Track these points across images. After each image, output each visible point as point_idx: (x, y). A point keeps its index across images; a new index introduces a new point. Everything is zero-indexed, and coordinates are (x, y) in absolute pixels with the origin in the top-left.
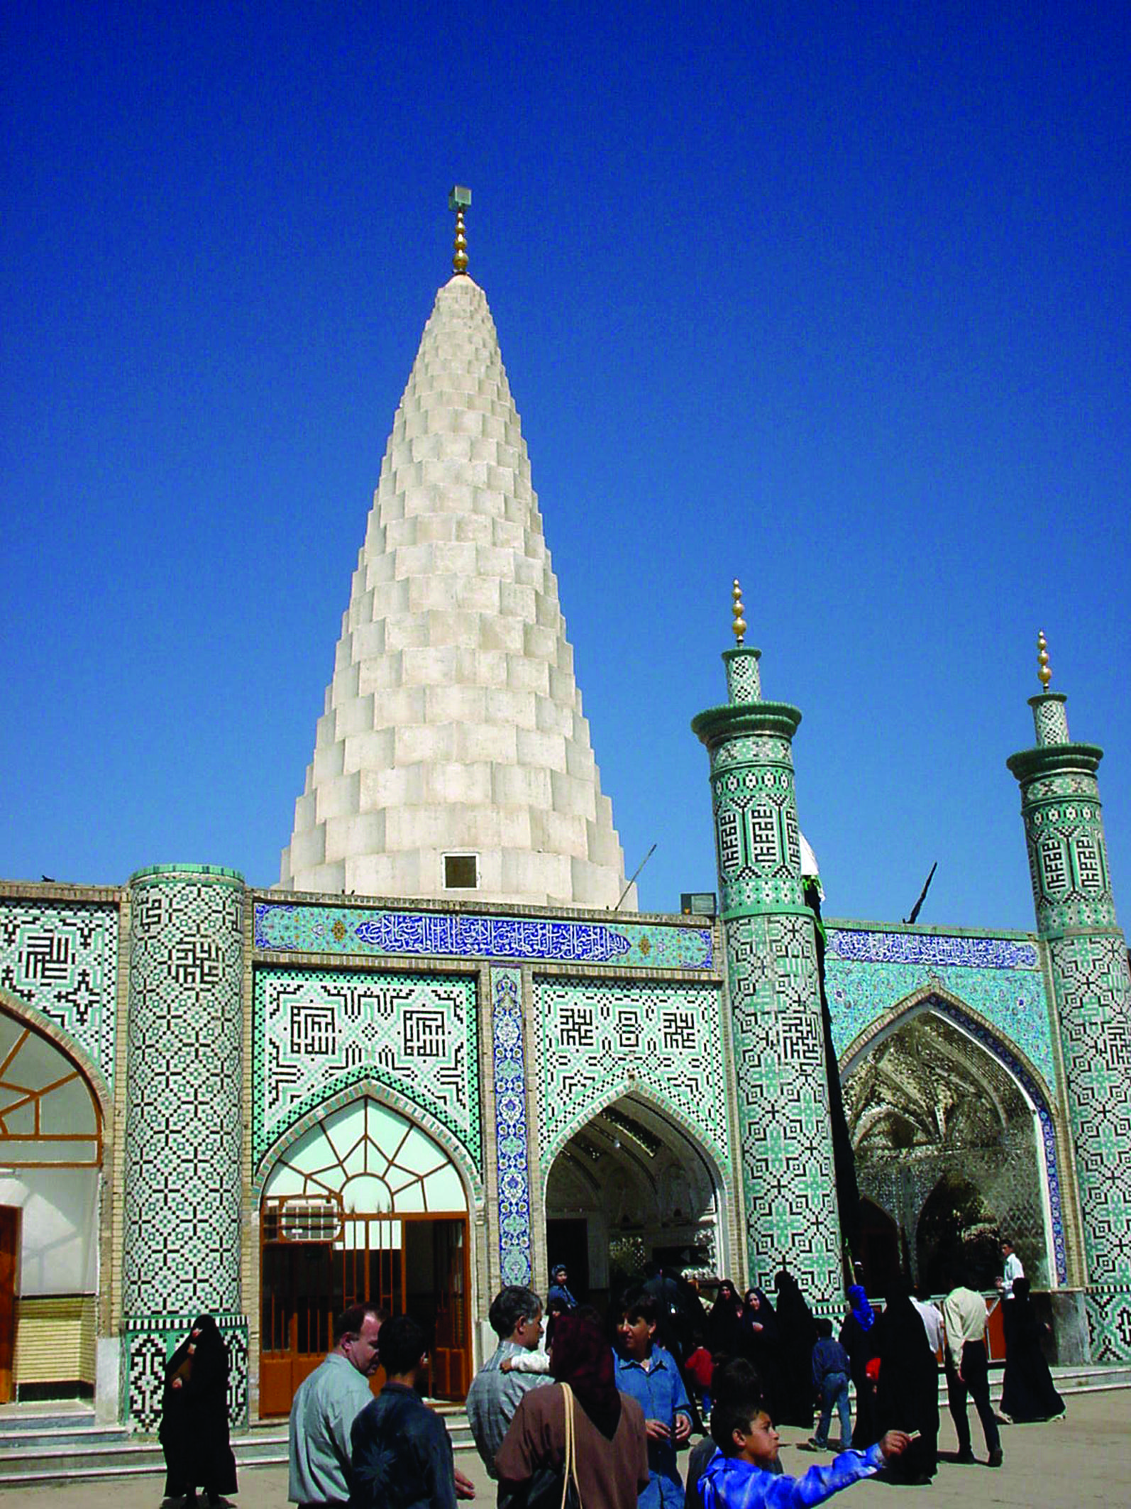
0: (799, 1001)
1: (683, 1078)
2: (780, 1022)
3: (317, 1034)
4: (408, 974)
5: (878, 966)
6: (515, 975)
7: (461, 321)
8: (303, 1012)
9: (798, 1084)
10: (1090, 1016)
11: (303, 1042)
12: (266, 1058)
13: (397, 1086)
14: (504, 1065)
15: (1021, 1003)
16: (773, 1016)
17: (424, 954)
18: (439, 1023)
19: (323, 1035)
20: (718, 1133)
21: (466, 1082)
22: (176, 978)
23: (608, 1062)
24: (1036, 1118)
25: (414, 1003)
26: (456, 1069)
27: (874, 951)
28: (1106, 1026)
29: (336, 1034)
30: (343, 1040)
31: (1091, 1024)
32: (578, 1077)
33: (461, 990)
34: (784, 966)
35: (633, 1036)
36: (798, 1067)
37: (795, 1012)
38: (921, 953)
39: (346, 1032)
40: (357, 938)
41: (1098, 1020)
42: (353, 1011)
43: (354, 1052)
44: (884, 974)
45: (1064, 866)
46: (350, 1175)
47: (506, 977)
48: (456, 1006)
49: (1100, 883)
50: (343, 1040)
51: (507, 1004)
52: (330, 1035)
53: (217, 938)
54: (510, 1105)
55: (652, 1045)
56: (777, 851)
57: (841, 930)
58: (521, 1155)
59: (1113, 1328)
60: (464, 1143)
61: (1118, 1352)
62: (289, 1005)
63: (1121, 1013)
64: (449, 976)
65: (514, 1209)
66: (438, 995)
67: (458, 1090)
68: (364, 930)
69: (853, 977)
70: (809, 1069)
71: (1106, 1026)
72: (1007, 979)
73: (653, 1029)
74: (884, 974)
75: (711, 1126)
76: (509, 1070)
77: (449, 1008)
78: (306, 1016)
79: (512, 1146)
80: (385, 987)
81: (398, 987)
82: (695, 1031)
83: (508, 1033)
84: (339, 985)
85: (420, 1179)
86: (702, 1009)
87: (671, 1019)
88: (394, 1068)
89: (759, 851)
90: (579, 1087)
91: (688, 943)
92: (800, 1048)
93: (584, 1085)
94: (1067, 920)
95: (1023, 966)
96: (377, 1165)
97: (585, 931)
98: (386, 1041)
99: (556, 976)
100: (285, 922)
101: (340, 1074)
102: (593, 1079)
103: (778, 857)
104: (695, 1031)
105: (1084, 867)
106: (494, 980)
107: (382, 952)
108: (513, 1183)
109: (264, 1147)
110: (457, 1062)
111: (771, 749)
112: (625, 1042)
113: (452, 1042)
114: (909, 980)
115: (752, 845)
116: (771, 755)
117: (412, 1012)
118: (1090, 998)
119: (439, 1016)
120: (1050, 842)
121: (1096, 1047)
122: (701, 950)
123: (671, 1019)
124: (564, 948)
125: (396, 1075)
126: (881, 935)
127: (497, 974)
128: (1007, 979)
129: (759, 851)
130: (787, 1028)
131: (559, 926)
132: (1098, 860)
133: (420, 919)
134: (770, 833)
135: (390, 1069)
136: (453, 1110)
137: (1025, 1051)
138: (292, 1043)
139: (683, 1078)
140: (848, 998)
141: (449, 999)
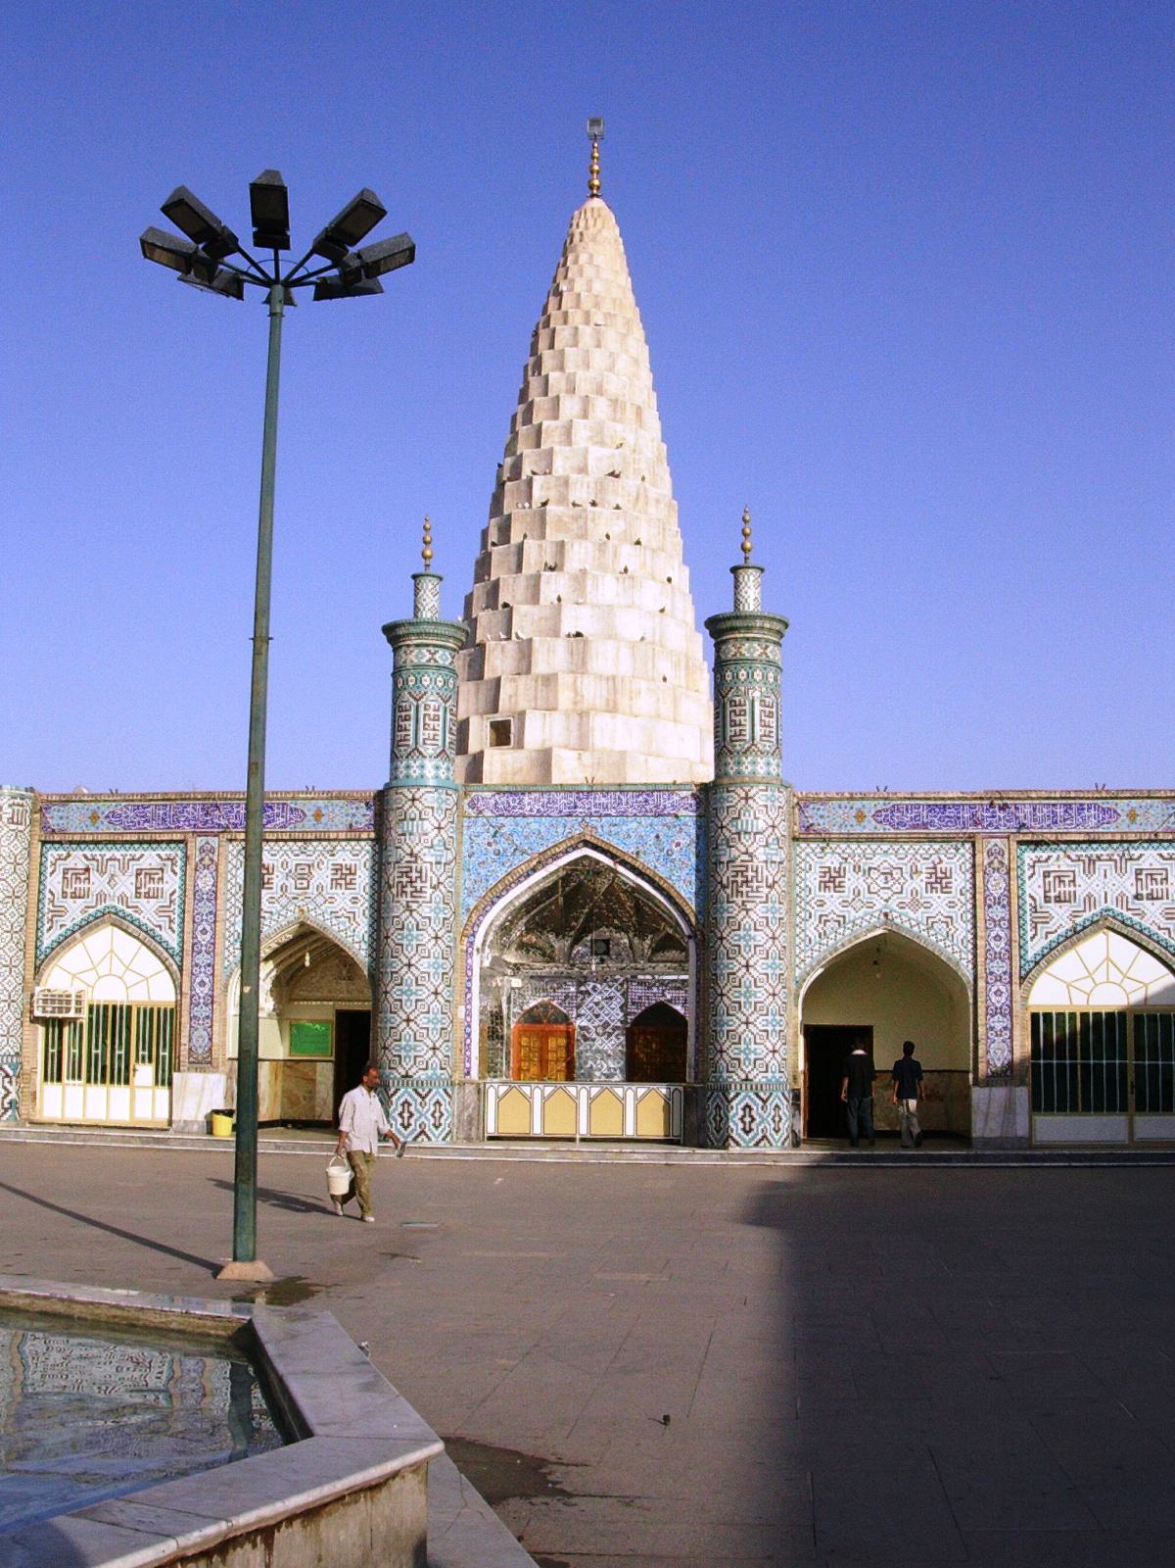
1: (939, 917)
3: (1155, 887)
5: (531, 819)
7: (600, 258)
10: (772, 855)
12: (46, 901)
13: (121, 914)
17: (151, 830)
23: (284, 901)
27: (528, 808)
29: (1169, 886)
31: (772, 862)
34: (403, 828)
35: (305, 882)
37: (407, 862)
38: (575, 807)
39: (97, 883)
40: (106, 822)
44: (534, 826)
46: (113, 972)
47: (208, 843)
50: (1081, 893)
51: (207, 861)
55: (321, 888)
56: (440, 738)
57: (499, 792)
58: (209, 965)
59: (446, 1115)
60: (172, 956)
61: (739, 1140)
63: (746, 853)
68: (112, 816)
72: (665, 825)
73: (322, 876)
74: (534, 826)
76: (205, 907)
78: (1055, 878)
79: (203, 959)
80: (124, 853)
81: (133, 852)
83: (205, 882)
84: (94, 853)
85: (74, 976)
87: (338, 868)
88: (128, 907)
94: (411, 772)
96: (119, 969)
97: (271, 807)
98: (123, 889)
100: (60, 814)
101: (91, 911)
102: (271, 913)
103: (440, 743)
106: (198, 846)
107: (122, 831)
108: (202, 984)
109: (42, 957)
110: (171, 902)
111: (417, 656)
112: (299, 886)
114: (560, 830)
120: (737, 699)
121: (721, 882)
122: (364, 815)
123: (338, 868)
125: (1128, 914)
126: (537, 795)
127: (201, 841)
128: (665, 825)
133: (149, 806)
135: (124, 908)
137: (676, 886)
138: (63, 892)
139: (939, 917)
140: (499, 847)
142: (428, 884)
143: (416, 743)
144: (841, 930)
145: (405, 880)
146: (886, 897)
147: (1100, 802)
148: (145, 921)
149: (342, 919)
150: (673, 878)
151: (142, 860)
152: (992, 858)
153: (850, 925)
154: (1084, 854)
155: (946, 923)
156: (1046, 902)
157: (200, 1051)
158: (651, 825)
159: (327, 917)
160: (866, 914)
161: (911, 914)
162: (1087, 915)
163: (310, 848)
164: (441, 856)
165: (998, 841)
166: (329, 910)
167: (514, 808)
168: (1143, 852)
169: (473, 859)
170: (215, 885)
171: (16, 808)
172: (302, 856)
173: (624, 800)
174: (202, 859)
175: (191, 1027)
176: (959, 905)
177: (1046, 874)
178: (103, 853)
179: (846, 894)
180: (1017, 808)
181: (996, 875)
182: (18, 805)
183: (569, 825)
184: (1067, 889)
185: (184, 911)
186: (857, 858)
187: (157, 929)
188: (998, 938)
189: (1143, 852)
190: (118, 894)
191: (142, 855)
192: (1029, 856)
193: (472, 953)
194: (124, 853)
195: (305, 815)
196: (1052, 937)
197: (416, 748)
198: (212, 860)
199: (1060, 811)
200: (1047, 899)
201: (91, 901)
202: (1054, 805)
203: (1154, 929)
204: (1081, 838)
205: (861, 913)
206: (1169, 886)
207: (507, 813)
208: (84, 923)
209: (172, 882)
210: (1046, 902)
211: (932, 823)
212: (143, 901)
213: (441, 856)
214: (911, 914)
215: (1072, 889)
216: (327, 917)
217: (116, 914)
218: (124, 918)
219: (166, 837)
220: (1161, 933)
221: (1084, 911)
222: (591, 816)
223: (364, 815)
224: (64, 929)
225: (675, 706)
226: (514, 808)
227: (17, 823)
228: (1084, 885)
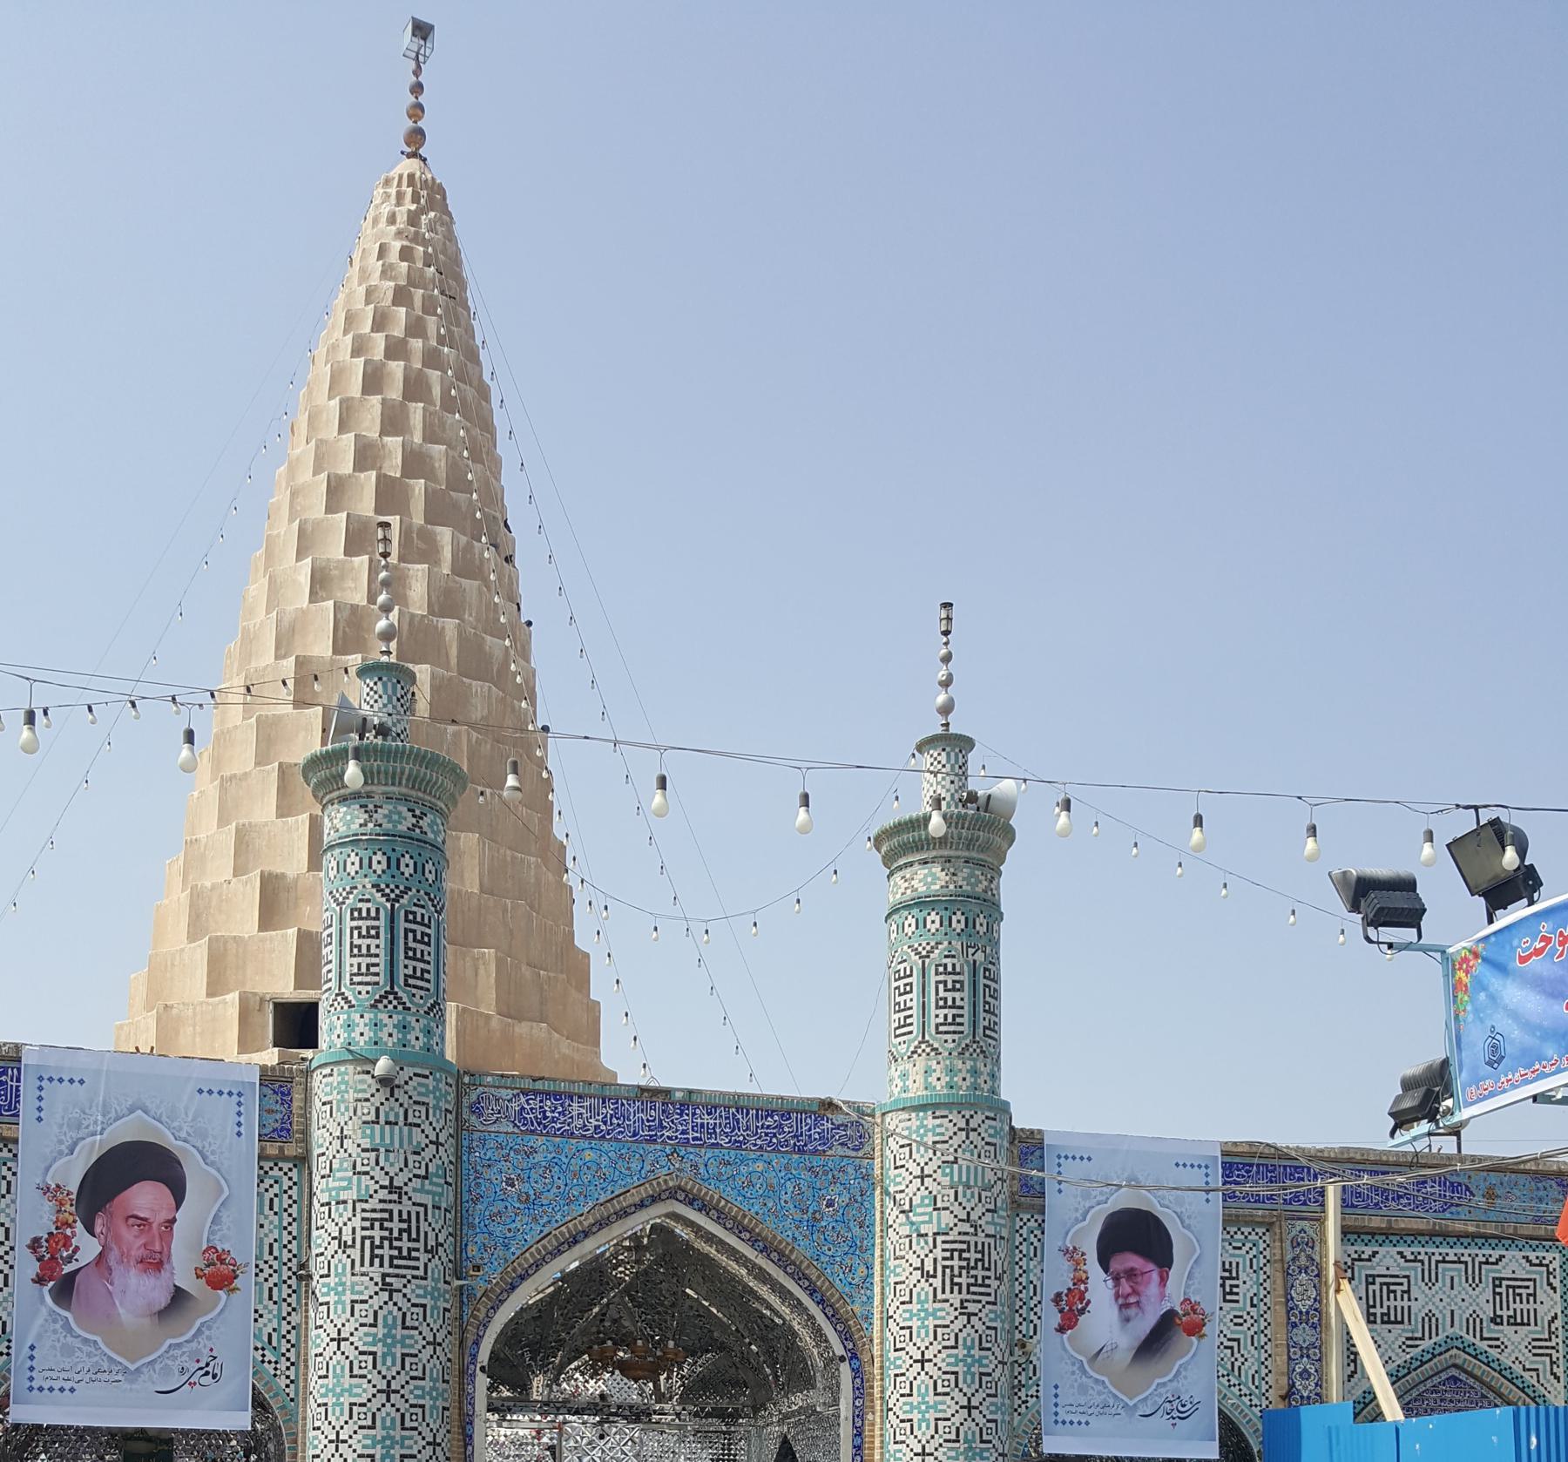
2: (359, 1216)
3: (1518, 1306)
5: (584, 1144)
16: (350, 1206)
18: (1531, 1291)
19: (1399, 1303)
24: (484, 1356)
27: (579, 1123)
28: (939, 1239)
31: (920, 1235)
34: (372, 1137)
36: (378, 1279)
44: (589, 1155)
45: (914, 1004)
48: (1549, 1273)
49: (431, 986)
51: (1303, 1261)
52: (1406, 1303)
54: (1305, 1374)
62: (1537, 1277)
66: (1403, 1257)
67: (1552, 1363)
69: (538, 1157)
70: (397, 1283)
71: (939, 1239)
74: (589, 1155)
75: (269, 1356)
77: (1488, 1271)
81: (1488, 1252)
82: (1240, 1282)
86: (271, 1194)
89: (941, 1020)
92: (963, 1280)
94: (411, 1037)
95: (841, 1151)
99: (1474, 1236)
104: (1240, 1282)
111: (388, 817)
113: (1544, 1313)
115: (348, 960)
116: (387, 826)
117: (1374, 1276)
118: (923, 1198)
119: (1531, 1284)
125: (1483, 1345)
129: (941, 1020)
130: (367, 1224)
132: (432, 949)
134: (426, 948)
140: (526, 1187)
141: (1541, 1265)
142: (421, 1245)
150: (823, 1258)
152: (1298, 1250)
155: (1231, 1348)
162: (1426, 1344)
164: (441, 1195)
167: (554, 1120)
168: (1503, 1252)
173: (743, 1122)
177: (1497, 1283)
179: (1241, 1304)
183: (651, 1157)
184: (1525, 1306)
188: (1305, 1374)
189: (1503, 1252)
193: (473, 1375)
203: (1518, 1369)
206: (1413, 1303)
207: (541, 1125)
213: (441, 1195)
220: (1526, 1375)
221: (1422, 1339)
226: (554, 1120)
228: (1423, 1300)
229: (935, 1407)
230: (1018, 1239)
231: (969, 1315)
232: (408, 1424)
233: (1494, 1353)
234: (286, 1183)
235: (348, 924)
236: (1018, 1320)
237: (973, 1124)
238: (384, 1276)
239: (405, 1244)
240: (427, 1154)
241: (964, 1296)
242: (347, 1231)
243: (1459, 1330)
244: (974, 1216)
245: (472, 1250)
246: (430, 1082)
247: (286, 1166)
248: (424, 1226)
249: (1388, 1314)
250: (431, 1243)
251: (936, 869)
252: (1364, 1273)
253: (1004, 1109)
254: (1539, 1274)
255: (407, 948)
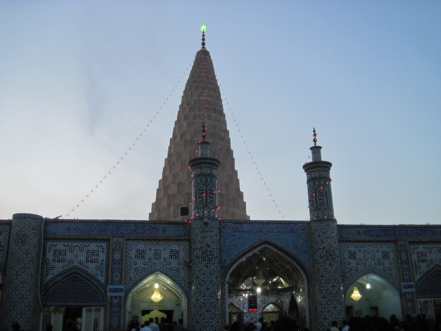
0: (330, 245)
1: (174, 268)
4: (89, 240)
5: (246, 233)
6: (121, 240)
8: (57, 251)
9: (205, 270)
11: (56, 259)
14: (116, 265)
15: (299, 243)
19: (62, 257)
20: (186, 284)
21: (104, 270)
22: (15, 243)
25: (90, 248)
26: (101, 266)
27: (245, 229)
29: (66, 257)
30: (429, 258)
31: (320, 249)
32: (140, 268)
33: (104, 245)
34: (203, 235)
35: (159, 256)
38: (262, 229)
41: (322, 247)
42: (431, 252)
43: (71, 262)
44: (247, 236)
47: (118, 240)
51: (118, 248)
53: (27, 232)
54: (406, 275)
57: (234, 223)
60: (102, 287)
64: (101, 240)
65: (116, 305)
69: (237, 237)
70: (209, 265)
72: (295, 236)
73: (165, 254)
74: (247, 236)
80: (82, 244)
81: (85, 244)
84: (68, 243)
88: (83, 266)
90: (140, 271)
91: (179, 229)
92: (330, 258)
93: (142, 270)
94: (210, 214)
97: (145, 227)
101: (66, 268)
105: (320, 199)
111: (205, 171)
114: (257, 237)
124: (137, 232)
125: (84, 268)
131: (136, 226)
135: (81, 266)
136: (99, 278)
138: (54, 260)
139: (174, 268)
141: (101, 247)
142: (213, 257)
143: (207, 203)
144: (357, 273)
145: (205, 255)
146: (370, 261)
147: (431, 229)
148: (90, 272)
149: (174, 271)
151: (89, 247)
152: (116, 245)
153: (359, 271)
154: (70, 244)
155: (137, 270)
156: (54, 262)
157: (115, 326)
158: (290, 236)
159: (168, 270)
160: (364, 267)
161: (378, 267)
162: (431, 266)
163: (161, 243)
165: (402, 241)
166: (169, 268)
167: (240, 229)
169: (225, 248)
170: (122, 257)
171: (36, 224)
172: (157, 246)
174: (116, 247)
175: (111, 316)
176: (132, 263)
177: (418, 253)
178: (72, 243)
180: (407, 231)
181: (403, 253)
182: (36, 222)
184: (425, 258)
185: (108, 268)
186: (360, 248)
187: (96, 275)
188: (406, 275)
190: (78, 261)
191: (89, 245)
192: (412, 247)
194: (82, 244)
195: (159, 230)
196: (422, 274)
197: (207, 205)
198: (120, 247)
199: (420, 231)
200: (419, 261)
201: (66, 263)
202: (418, 230)
204: (427, 240)
205: (363, 267)
208: (63, 273)
209: (102, 256)
210: (54, 262)
211: (382, 235)
212: (90, 264)
214: (378, 267)
215: (426, 258)
216: (168, 270)
217: (78, 269)
218: (81, 271)
219: (101, 238)
222: (268, 232)
223: (183, 231)
224: (54, 275)
225: (227, 189)
226: (240, 229)
227: (36, 230)
228: (429, 257)
229: (321, 287)
230: (341, 248)
231: (332, 266)
232: (212, 295)
233: (87, 269)
234: (186, 245)
235: (198, 192)
236: (342, 266)
237: (329, 224)
238: (206, 264)
239: (210, 257)
240: (214, 237)
241: (330, 261)
242: (198, 255)
243: (438, 263)
244: (331, 244)
245: (224, 257)
246: (215, 223)
247: (186, 242)
248: (214, 253)
249: (59, 260)
250: (216, 256)
251: (199, 169)
252: (53, 249)
253: (335, 221)
254: (53, 248)
255: (209, 196)
